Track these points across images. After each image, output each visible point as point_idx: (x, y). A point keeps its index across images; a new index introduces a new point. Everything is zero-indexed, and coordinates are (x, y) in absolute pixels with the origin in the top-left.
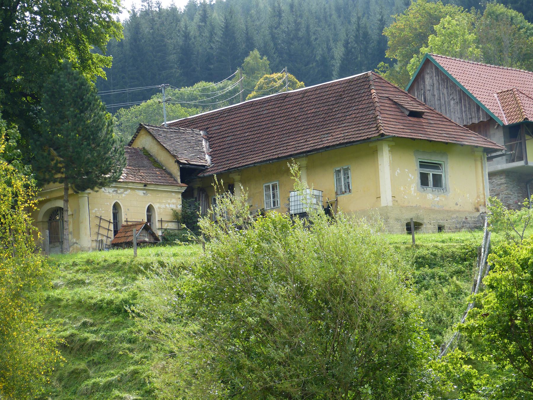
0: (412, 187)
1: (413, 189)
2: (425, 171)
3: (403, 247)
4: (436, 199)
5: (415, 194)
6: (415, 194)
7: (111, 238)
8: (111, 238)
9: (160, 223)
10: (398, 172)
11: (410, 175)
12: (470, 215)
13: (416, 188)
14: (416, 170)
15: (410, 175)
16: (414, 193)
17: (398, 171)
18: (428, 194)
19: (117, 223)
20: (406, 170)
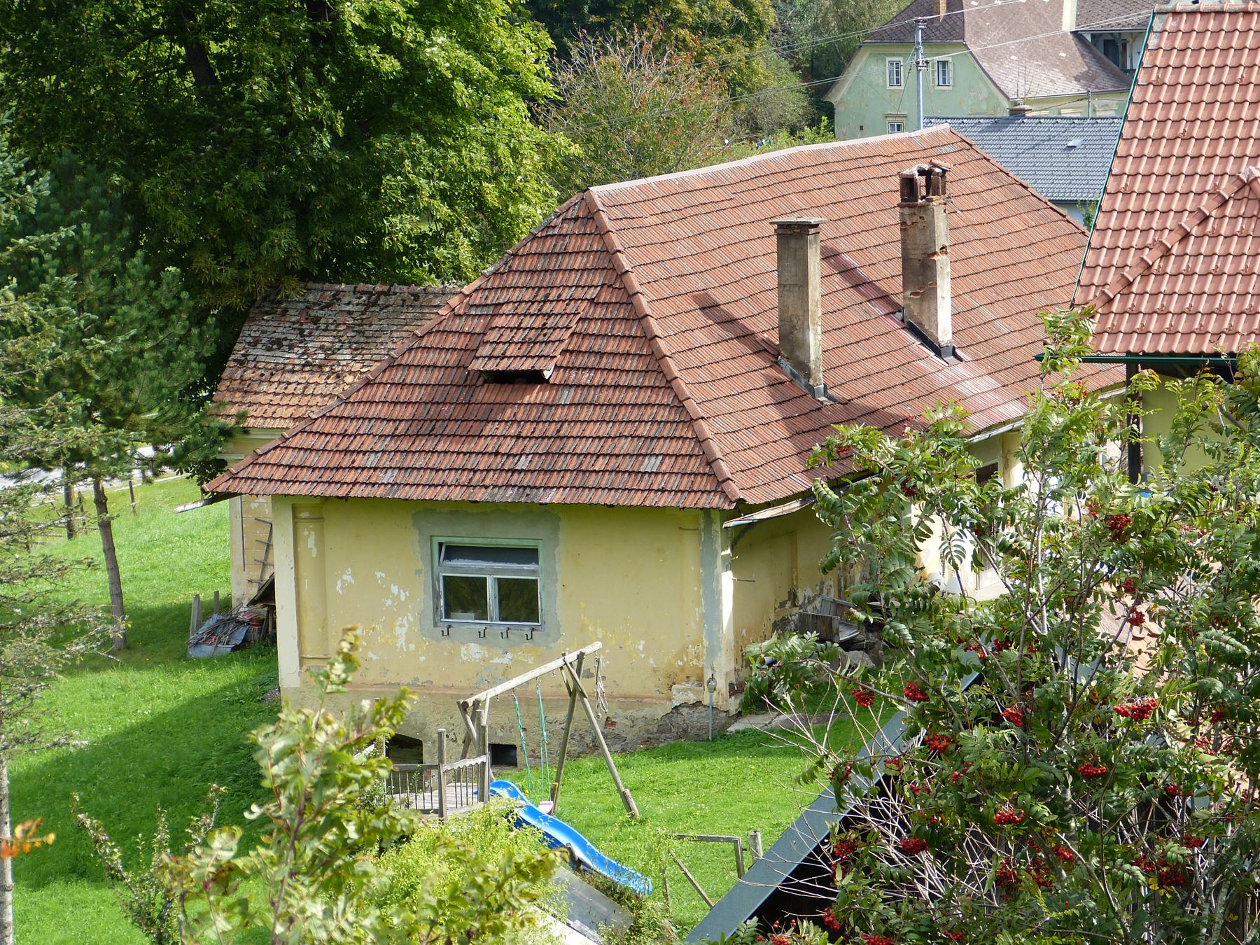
0: (402, 626)
1: (401, 632)
2: (466, 568)
3: (198, 851)
4: (496, 660)
5: (412, 647)
6: (412, 647)
7: (977, 588)
8: (977, 588)
9: (269, 560)
10: (343, 582)
11: (395, 589)
12: (629, 713)
13: (416, 629)
14: (418, 572)
15: (395, 589)
16: (408, 642)
17: (345, 577)
18: (463, 644)
19: (759, 21)
20: (379, 574)
